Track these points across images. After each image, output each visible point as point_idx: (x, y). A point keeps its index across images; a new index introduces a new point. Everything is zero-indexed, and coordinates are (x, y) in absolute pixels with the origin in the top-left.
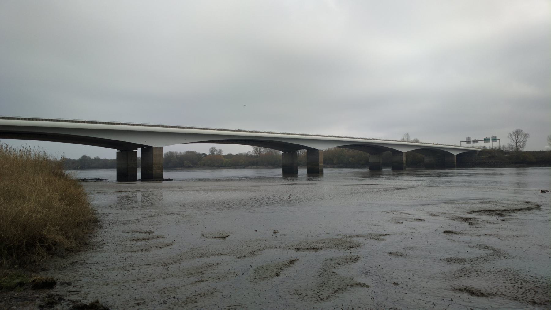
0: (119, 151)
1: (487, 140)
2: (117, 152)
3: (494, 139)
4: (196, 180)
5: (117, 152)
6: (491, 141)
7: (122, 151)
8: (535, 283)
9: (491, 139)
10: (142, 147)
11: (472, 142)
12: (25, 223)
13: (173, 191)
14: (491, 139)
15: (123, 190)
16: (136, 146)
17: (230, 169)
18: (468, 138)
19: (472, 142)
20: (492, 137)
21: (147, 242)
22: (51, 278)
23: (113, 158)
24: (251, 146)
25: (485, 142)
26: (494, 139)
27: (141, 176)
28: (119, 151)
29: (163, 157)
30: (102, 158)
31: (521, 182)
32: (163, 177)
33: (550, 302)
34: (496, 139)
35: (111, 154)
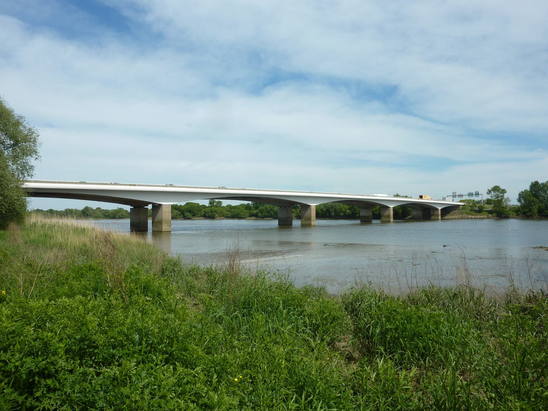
0: (132, 207)
1: (470, 194)
4: (111, 215)
7: (135, 207)
9: (474, 194)
10: (154, 204)
11: (457, 197)
12: (28, 149)
14: (474, 194)
16: (147, 203)
18: (454, 192)
19: (457, 197)
21: (238, 323)
22: (30, 129)
28: (132, 207)
30: (78, 209)
31: (460, 216)
33: (547, 294)
34: (478, 194)
35: (128, 208)
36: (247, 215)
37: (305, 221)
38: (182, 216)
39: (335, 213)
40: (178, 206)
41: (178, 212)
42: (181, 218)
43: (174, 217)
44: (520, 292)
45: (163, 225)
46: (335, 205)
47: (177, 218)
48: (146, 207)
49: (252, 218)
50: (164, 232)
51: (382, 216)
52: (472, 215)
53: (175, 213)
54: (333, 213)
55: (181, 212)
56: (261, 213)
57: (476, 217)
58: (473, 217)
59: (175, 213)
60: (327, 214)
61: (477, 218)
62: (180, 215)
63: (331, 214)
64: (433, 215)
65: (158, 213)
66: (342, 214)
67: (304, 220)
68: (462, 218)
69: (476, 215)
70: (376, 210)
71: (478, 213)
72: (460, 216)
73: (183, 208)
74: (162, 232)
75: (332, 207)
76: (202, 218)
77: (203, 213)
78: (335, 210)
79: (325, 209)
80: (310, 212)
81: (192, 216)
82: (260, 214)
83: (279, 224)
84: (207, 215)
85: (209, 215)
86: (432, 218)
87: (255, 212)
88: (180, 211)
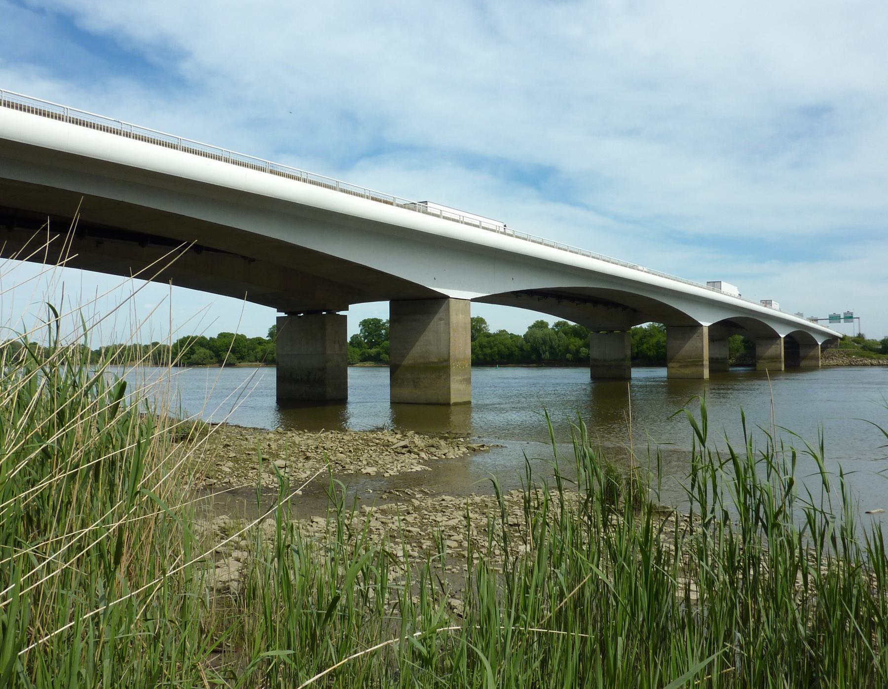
0: (283, 314)
1: (834, 318)
2: (278, 318)
3: (849, 317)
5: (278, 318)
6: (842, 321)
8: (294, 434)
9: (842, 316)
13: (781, 490)
14: (842, 316)
15: (729, 531)
17: (519, 368)
20: (845, 314)
23: (251, 334)
24: (389, 319)
25: (830, 323)
26: (849, 317)
27: (275, 385)
28: (283, 314)
29: (350, 335)
31: (847, 361)
32: (280, 379)
34: (851, 317)
36: (357, 357)
37: (680, 367)
38: (215, 360)
39: (550, 353)
40: (206, 339)
41: (207, 351)
42: (213, 363)
43: (200, 361)
44: (487, 454)
45: (452, 378)
46: (550, 339)
47: (205, 364)
48: (341, 313)
49: (368, 364)
50: (456, 404)
51: (760, 358)
52: (872, 358)
53: (202, 354)
54: (547, 353)
55: (214, 351)
56: (387, 353)
57: (881, 362)
58: (874, 362)
59: (202, 354)
60: (534, 357)
61: (882, 365)
62: (212, 359)
63: (543, 356)
64: (804, 358)
65: (424, 330)
66: (569, 356)
67: (678, 364)
68: (850, 365)
69: (879, 359)
70: (647, 348)
71: (882, 354)
72: (847, 361)
73: (218, 344)
74: (448, 404)
75: (544, 342)
76: (258, 363)
77: (260, 354)
78: (551, 347)
79: (527, 347)
80: (700, 345)
81: (238, 359)
82: (384, 356)
83: (592, 377)
84: (270, 357)
85: (273, 358)
86: (803, 363)
87: (374, 351)
88: (210, 348)
